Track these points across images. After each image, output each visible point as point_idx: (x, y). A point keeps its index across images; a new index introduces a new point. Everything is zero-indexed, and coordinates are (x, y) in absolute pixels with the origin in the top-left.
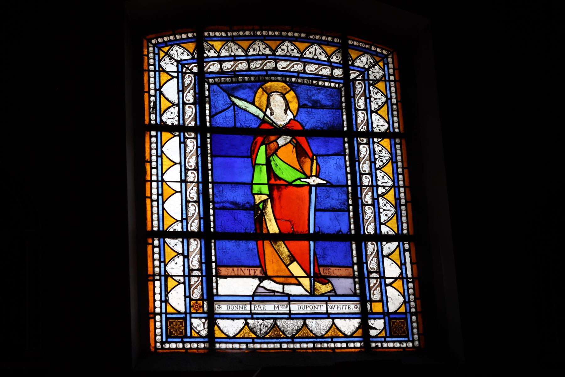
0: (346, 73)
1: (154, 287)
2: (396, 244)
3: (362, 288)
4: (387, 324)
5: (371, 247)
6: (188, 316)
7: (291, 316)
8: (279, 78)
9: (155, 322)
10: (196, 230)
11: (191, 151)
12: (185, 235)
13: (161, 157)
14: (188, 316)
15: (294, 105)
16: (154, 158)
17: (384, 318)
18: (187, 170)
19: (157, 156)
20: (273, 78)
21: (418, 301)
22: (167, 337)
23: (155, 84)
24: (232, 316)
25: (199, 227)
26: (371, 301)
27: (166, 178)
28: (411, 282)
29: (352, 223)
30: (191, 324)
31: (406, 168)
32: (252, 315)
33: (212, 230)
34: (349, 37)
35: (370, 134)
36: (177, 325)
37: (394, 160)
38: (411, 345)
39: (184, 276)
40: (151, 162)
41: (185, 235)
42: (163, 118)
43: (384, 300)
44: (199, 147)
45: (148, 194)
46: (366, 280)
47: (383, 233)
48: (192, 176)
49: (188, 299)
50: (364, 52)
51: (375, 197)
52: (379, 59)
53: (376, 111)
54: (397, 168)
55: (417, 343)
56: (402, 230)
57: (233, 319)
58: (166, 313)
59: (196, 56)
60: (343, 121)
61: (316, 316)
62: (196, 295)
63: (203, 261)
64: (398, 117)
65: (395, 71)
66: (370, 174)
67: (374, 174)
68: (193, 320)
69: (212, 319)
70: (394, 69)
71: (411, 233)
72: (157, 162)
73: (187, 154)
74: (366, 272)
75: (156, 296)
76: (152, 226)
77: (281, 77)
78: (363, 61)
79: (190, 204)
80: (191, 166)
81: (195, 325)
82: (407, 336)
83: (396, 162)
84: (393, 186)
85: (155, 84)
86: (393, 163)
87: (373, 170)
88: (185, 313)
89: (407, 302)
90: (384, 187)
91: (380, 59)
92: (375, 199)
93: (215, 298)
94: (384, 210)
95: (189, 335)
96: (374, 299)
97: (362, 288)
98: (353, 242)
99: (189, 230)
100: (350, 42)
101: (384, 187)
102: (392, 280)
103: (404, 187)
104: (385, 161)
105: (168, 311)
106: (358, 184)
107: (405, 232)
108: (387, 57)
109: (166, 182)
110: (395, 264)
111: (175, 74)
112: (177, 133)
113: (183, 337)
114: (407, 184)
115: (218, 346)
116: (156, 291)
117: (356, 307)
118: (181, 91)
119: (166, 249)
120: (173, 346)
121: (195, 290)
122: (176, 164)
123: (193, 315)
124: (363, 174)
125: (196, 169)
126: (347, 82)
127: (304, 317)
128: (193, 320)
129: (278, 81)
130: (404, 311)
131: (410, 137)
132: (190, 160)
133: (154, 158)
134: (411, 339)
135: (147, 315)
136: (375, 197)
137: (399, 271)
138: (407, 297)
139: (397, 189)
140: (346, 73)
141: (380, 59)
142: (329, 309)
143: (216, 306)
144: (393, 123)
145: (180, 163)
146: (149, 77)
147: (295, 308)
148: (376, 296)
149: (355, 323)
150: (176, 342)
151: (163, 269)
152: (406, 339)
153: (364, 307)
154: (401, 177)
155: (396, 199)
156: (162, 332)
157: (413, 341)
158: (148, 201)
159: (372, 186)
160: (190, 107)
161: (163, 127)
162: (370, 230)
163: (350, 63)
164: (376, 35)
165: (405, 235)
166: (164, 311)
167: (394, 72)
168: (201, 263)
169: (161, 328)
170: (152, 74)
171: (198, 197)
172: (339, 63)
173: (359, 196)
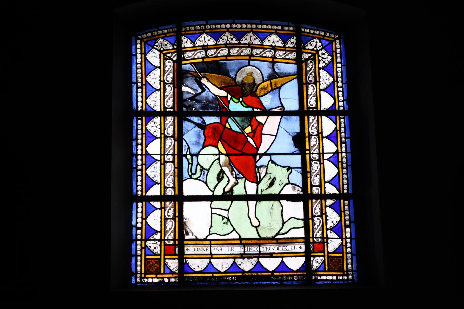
1: (137, 207)
9: (136, 245)
11: (169, 178)
21: (345, 102)
23: (142, 129)
28: (342, 118)
30: (165, 264)
31: (348, 138)
34: (302, 25)
36: (154, 266)
39: (161, 155)
40: (137, 139)
42: (148, 101)
44: (176, 168)
45: (134, 80)
49: (162, 83)
59: (176, 47)
64: (347, 179)
65: (351, 224)
68: (167, 261)
69: (181, 257)
70: (350, 220)
71: (351, 192)
72: (142, 223)
74: (306, 106)
75: (138, 219)
76: (137, 107)
80: (170, 139)
81: (169, 264)
95: (162, 272)
100: (303, 30)
103: (346, 153)
104: (327, 62)
107: (346, 191)
113: (157, 272)
116: (138, 211)
117: (301, 248)
120: (150, 280)
121: (170, 144)
125: (174, 218)
128: (167, 261)
132: (169, 101)
135: (129, 255)
138: (339, 149)
143: (186, 248)
144: (340, 123)
145: (160, 183)
146: (136, 49)
149: (302, 260)
150: (152, 278)
156: (142, 173)
157: (347, 275)
158: (134, 88)
162: (316, 191)
164: (326, 23)
165: (346, 194)
167: (342, 85)
169: (142, 186)
171: (174, 184)
172: (294, 47)
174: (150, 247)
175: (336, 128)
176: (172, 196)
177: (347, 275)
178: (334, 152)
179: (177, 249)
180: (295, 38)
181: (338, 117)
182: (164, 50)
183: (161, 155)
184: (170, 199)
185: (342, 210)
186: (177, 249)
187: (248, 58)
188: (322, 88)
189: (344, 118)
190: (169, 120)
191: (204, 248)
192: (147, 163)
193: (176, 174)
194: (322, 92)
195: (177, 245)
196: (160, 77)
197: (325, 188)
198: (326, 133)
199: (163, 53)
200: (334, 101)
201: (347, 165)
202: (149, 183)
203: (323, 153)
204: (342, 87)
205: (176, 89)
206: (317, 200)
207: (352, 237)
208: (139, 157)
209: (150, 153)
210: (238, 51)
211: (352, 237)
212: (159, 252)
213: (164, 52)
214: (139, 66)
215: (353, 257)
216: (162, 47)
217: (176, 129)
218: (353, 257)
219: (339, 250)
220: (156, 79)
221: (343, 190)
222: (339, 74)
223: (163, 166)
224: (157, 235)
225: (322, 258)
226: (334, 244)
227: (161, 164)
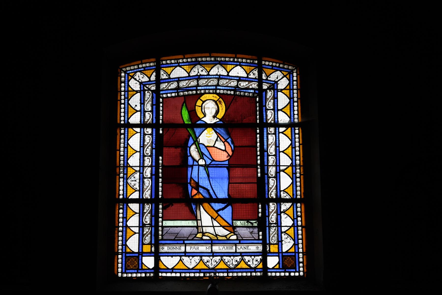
0: (260, 85)
2: (290, 204)
3: (264, 235)
4: (281, 260)
5: (272, 206)
8: (211, 91)
10: (149, 198)
13: (127, 148)
15: (220, 115)
16: (122, 149)
17: (279, 256)
18: (144, 156)
19: (124, 147)
20: (207, 91)
24: (172, 255)
26: (270, 244)
27: (129, 224)
29: (258, 141)
32: (186, 254)
33: (161, 121)
35: (276, 125)
36: (134, 260)
37: (294, 146)
38: (297, 274)
39: (140, 166)
43: (280, 242)
44: (153, 216)
46: (267, 228)
47: (282, 197)
50: (275, 69)
51: (278, 171)
53: (282, 106)
54: (295, 151)
55: (302, 274)
56: (297, 195)
57: (172, 256)
60: (257, 143)
61: (229, 254)
66: (275, 155)
67: (278, 155)
69: (157, 256)
72: (124, 152)
77: (212, 81)
78: (275, 76)
82: (295, 269)
83: (295, 147)
84: (293, 225)
85: (124, 143)
86: (292, 148)
87: (278, 153)
89: (296, 245)
91: (287, 73)
92: (278, 173)
93: (160, 242)
96: (272, 243)
97: (264, 235)
98: (262, 273)
99: (144, 198)
102: (287, 228)
108: (292, 71)
109: (129, 227)
110: (289, 217)
111: (138, 169)
114: (304, 224)
115: (160, 274)
118: (142, 147)
122: (137, 152)
126: (260, 92)
127: (222, 255)
129: (210, 93)
130: (294, 251)
131: (308, 127)
133: (122, 149)
134: (297, 270)
136: (278, 171)
137: (291, 162)
138: (294, 162)
139: (296, 228)
140: (260, 85)
141: (287, 73)
147: (216, 248)
148: (274, 240)
152: (294, 270)
153: (264, 248)
154: (295, 82)
155: (293, 173)
157: (299, 272)
164: (285, 58)
168: (151, 174)
172: (255, 78)
173: (264, 104)
176: (146, 128)
177: (299, 272)
178: (291, 225)
180: (257, 70)
183: (140, 166)
184: (147, 201)
187: (215, 87)
188: (280, 131)
190: (147, 207)
191: (174, 247)
196: (141, 100)
201: (298, 99)
204: (300, 177)
205: (153, 218)
206: (271, 123)
208: (123, 93)
209: (131, 165)
210: (206, 82)
214: (122, 136)
215: (304, 256)
218: (304, 256)
220: (135, 181)
221: (294, 119)
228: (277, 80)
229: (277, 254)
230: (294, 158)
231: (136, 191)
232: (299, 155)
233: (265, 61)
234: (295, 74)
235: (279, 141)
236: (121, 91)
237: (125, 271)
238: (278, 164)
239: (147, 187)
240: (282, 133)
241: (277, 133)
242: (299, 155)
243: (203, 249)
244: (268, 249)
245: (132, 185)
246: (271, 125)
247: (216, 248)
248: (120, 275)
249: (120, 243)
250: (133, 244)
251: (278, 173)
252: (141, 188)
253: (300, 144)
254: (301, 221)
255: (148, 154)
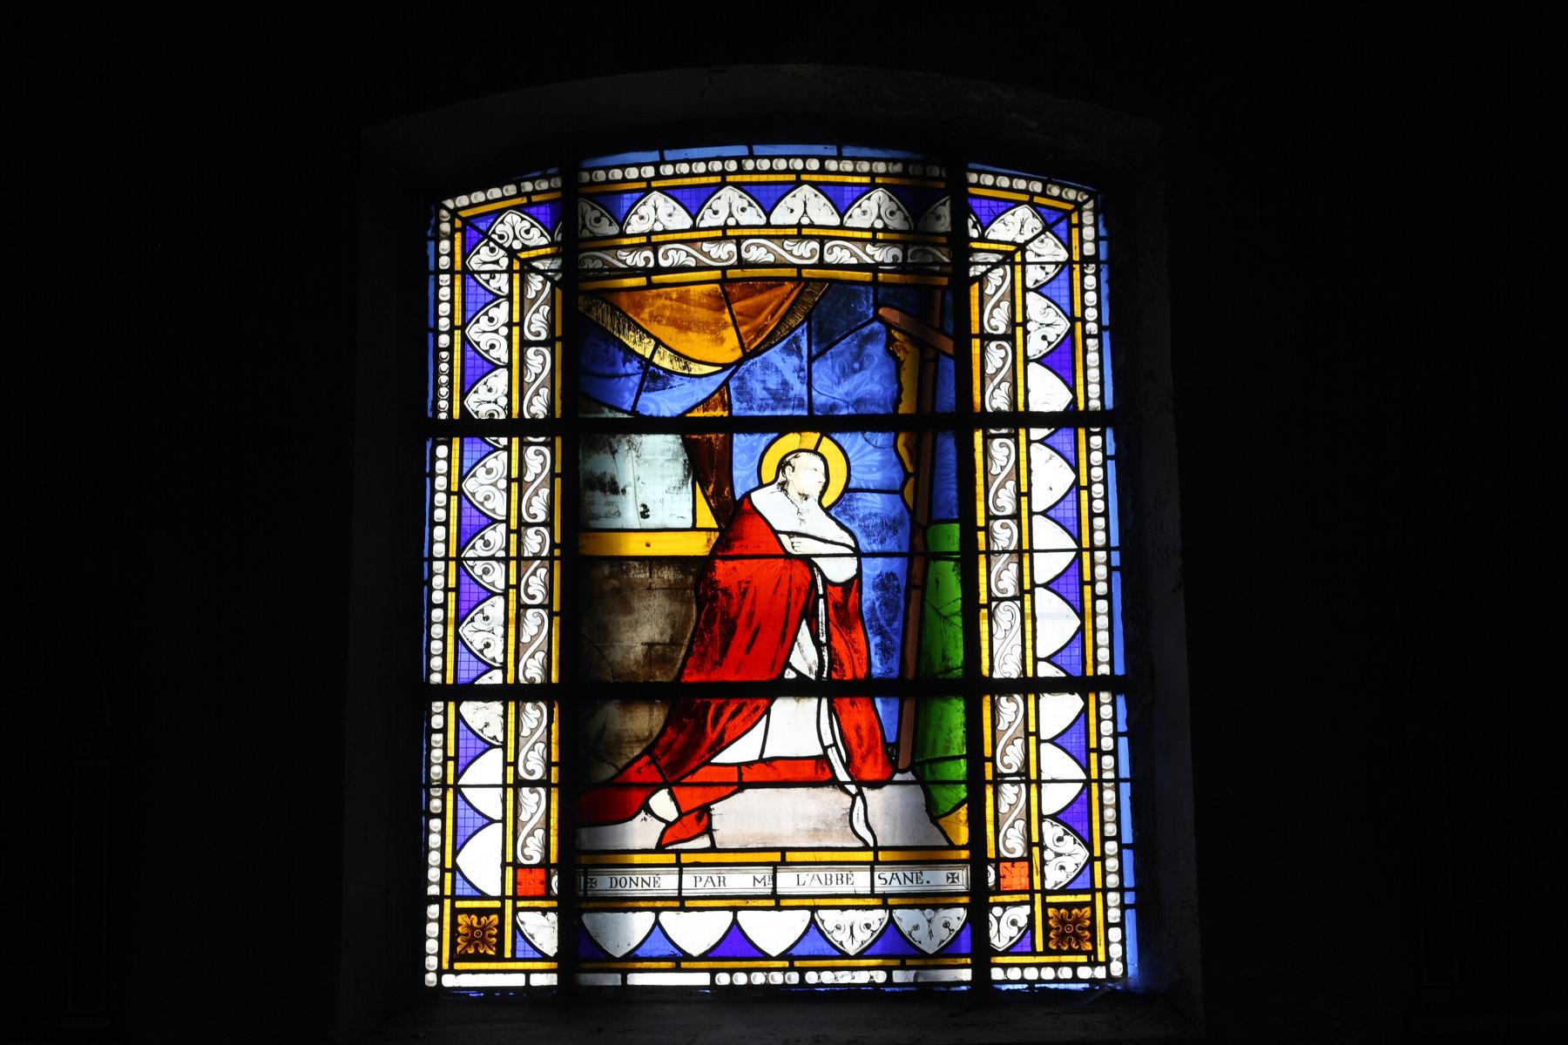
6: (509, 903)
7: (777, 901)
12: (513, 694)
14: (509, 903)
22: (452, 961)
25: (551, 407)
28: (1095, 434)
41: (513, 694)
48: (534, 542)
52: (1055, 222)
55: (1117, 969)
58: (454, 898)
62: (532, 851)
63: (555, 758)
73: (521, 740)
79: (531, 352)
81: (527, 929)
88: (502, 898)
90: (1042, 265)
92: (1024, 592)
94: (1058, 855)
99: (527, 416)
101: (1042, 265)
105: (459, 892)
106: (982, 547)
112: (504, 441)
119: (461, 814)
121: (535, 724)
123: (520, 904)
124: (996, 518)
134: (1101, 958)
136: (1027, 586)
142: (878, 882)
151: (456, 405)
159: (1019, 552)
160: (538, 453)
161: (472, 428)
162: (998, 400)
163: (974, 233)
166: (448, 892)
170: (445, 278)
174: (473, 494)
175: (1077, 482)
179: (555, 879)
181: (1082, 432)
182: (525, 248)
185: (1087, 577)
186: (555, 879)
189: (1102, 434)
192: (462, 752)
193: (554, 822)
194: (1032, 366)
195: (553, 866)
197: (1025, 308)
198: (1042, 499)
199: (519, 259)
200: (1078, 622)
201: (1101, 328)
202: (471, 519)
203: (1031, 551)
207: (1126, 885)
211: (1126, 885)
212: (505, 359)
213: (523, 255)
216: (515, 238)
217: (554, 840)
219: (1084, 882)
222: (1091, 297)
223: (513, 537)
224: (498, 306)
225: (1026, 909)
226: (1065, 859)
227: (509, 531)
228: (1020, 240)
229: (1027, 897)
230: (1088, 605)
231: (492, 746)
232: (1105, 514)
233: (980, 172)
234: (1088, 218)
235: (1027, 391)
236: (432, 559)
237: (451, 965)
238: (1026, 546)
239: (537, 393)
240: (1042, 441)
241: (1025, 514)
242: (1105, 514)
243: (740, 882)
244: (991, 879)
245: (484, 346)
246: (1008, 687)
247: (788, 882)
248: (431, 978)
249: (441, 482)
250: (482, 863)
251: (1024, 592)
252: (511, 735)
253: (1106, 458)
254: (1107, 530)
255: (536, 354)
